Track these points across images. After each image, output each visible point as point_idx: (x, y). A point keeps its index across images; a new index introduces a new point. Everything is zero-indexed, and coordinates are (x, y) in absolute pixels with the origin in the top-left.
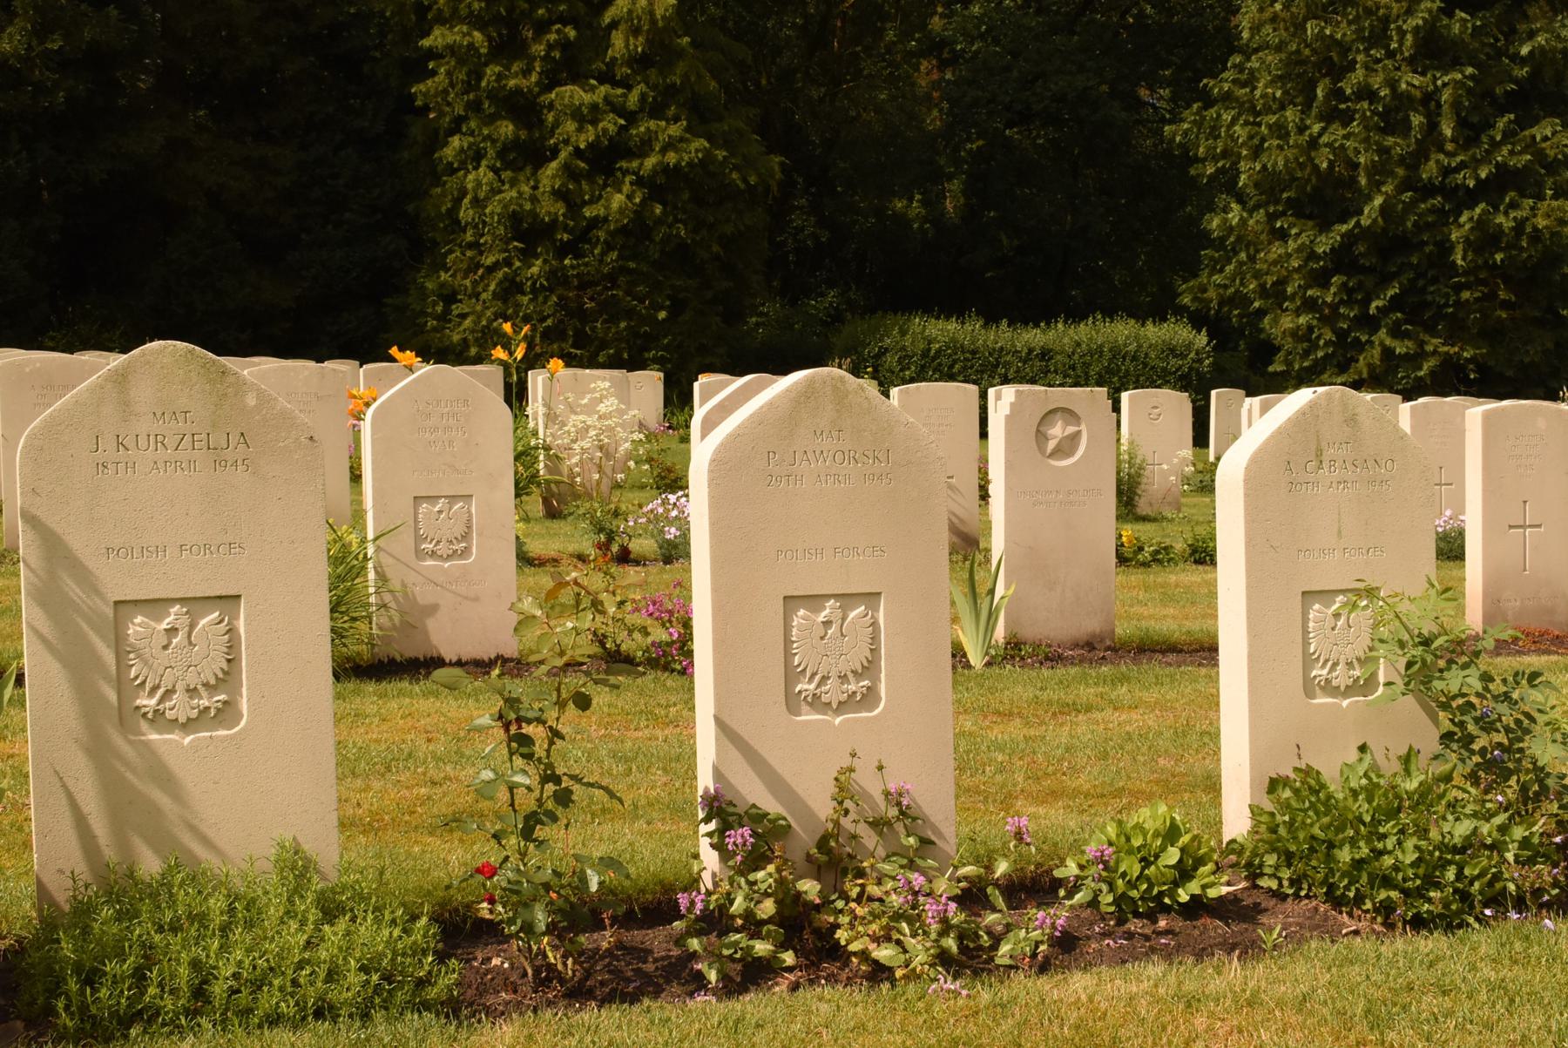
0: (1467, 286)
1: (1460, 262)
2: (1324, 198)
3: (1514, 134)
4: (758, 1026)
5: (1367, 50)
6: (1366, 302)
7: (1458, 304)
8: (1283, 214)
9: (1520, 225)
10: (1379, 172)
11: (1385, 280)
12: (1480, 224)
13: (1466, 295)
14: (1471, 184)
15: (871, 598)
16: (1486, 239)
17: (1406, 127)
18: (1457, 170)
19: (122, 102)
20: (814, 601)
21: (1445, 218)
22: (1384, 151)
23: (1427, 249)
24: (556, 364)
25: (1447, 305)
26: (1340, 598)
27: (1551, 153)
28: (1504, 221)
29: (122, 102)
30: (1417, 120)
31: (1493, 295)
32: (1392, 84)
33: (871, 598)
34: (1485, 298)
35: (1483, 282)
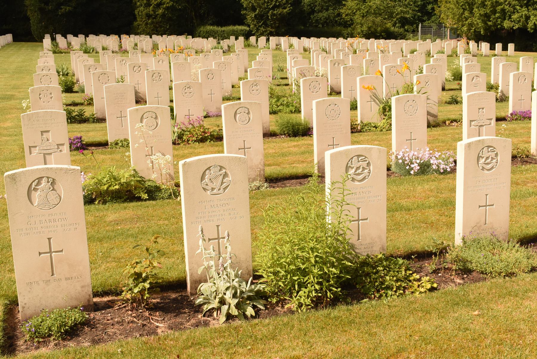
2: (254, 9)
15: (483, 108)
16: (273, 15)
21: (268, 12)
28: (275, 12)
33: (483, 108)
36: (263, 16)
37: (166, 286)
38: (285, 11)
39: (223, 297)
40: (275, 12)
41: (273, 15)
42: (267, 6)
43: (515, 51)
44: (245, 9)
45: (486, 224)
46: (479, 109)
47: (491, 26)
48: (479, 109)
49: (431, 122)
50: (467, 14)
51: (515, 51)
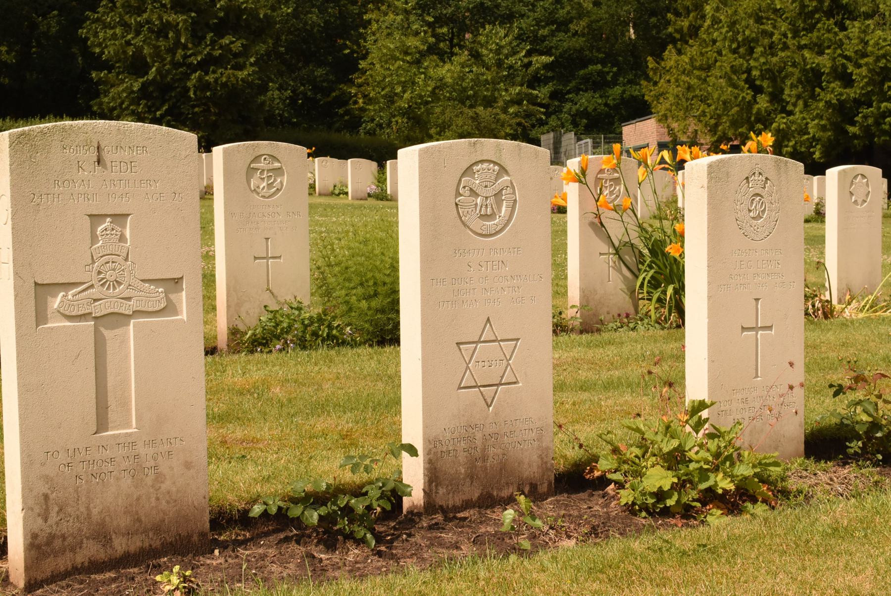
0: (198, 106)
1: (192, 96)
2: (137, 66)
3: (216, 41)
4: (657, 433)
5: (152, 3)
6: (155, 112)
7: (194, 114)
8: (123, 72)
9: (216, 80)
10: (157, 54)
11: (163, 104)
12: (200, 79)
13: (196, 109)
14: (196, 62)
15: (119, 218)
16: (203, 86)
17: (166, 37)
18: (190, 56)
19: (193, 14)
20: (101, 217)
21: (187, 76)
22: (157, 47)
23: (178, 90)
24: (773, 139)
25: (189, 114)
26: (108, 219)
27: (234, 49)
28: (210, 78)
29: (193, 14)
30: (171, 35)
31: (208, 110)
32: (160, 18)
33: (119, 218)
34: (204, 111)
35: (205, 104)
36: (169, 88)
37: (135, 554)
38: (242, 74)
39: (748, 512)
40: (210, 78)
41: (203, 86)
42: (185, 57)
43: (806, 173)
44: (107, 66)
45: (757, 376)
46: (96, 218)
47: (855, 136)
48: (96, 218)
49: (808, 294)
50: (763, 103)
51: (806, 173)
